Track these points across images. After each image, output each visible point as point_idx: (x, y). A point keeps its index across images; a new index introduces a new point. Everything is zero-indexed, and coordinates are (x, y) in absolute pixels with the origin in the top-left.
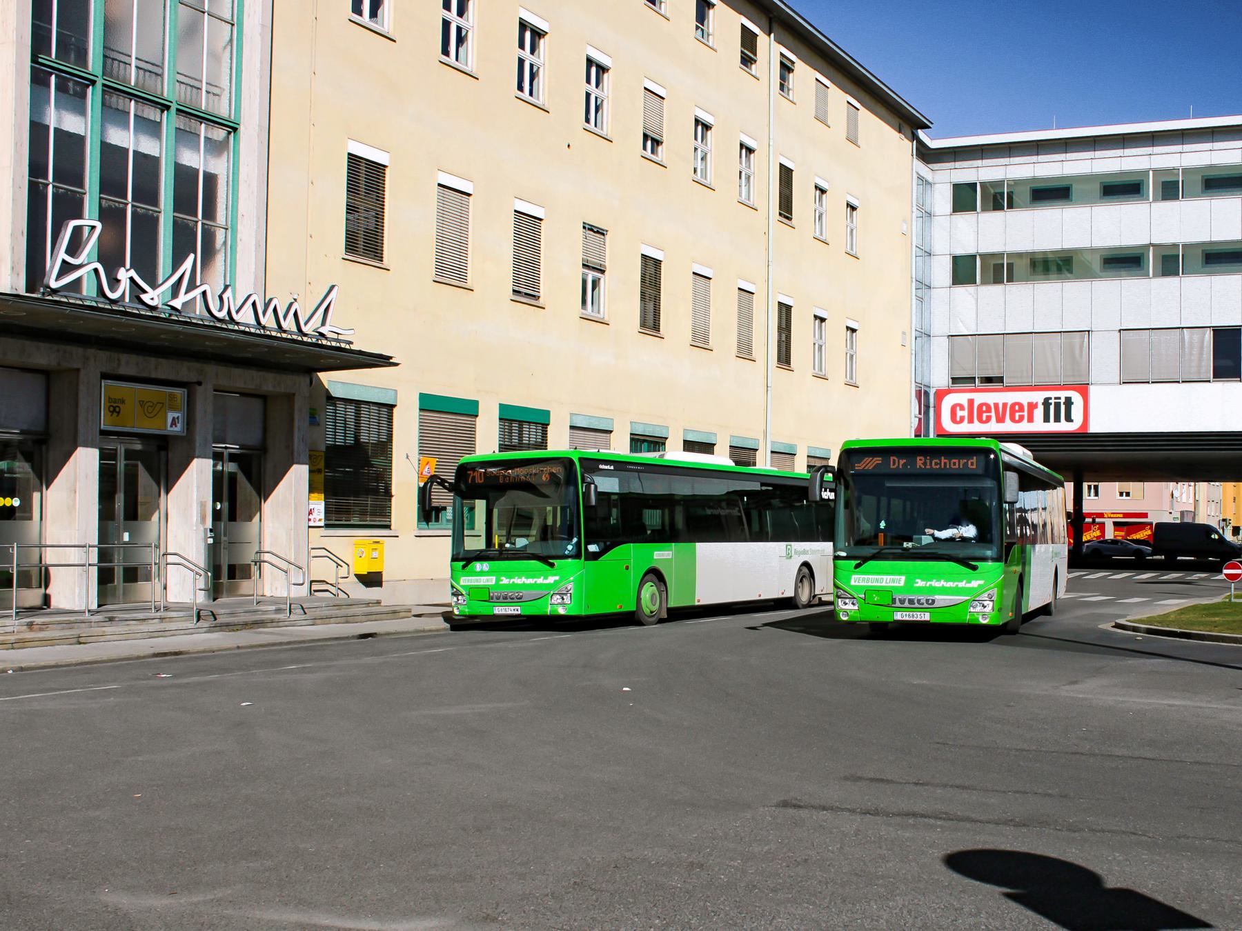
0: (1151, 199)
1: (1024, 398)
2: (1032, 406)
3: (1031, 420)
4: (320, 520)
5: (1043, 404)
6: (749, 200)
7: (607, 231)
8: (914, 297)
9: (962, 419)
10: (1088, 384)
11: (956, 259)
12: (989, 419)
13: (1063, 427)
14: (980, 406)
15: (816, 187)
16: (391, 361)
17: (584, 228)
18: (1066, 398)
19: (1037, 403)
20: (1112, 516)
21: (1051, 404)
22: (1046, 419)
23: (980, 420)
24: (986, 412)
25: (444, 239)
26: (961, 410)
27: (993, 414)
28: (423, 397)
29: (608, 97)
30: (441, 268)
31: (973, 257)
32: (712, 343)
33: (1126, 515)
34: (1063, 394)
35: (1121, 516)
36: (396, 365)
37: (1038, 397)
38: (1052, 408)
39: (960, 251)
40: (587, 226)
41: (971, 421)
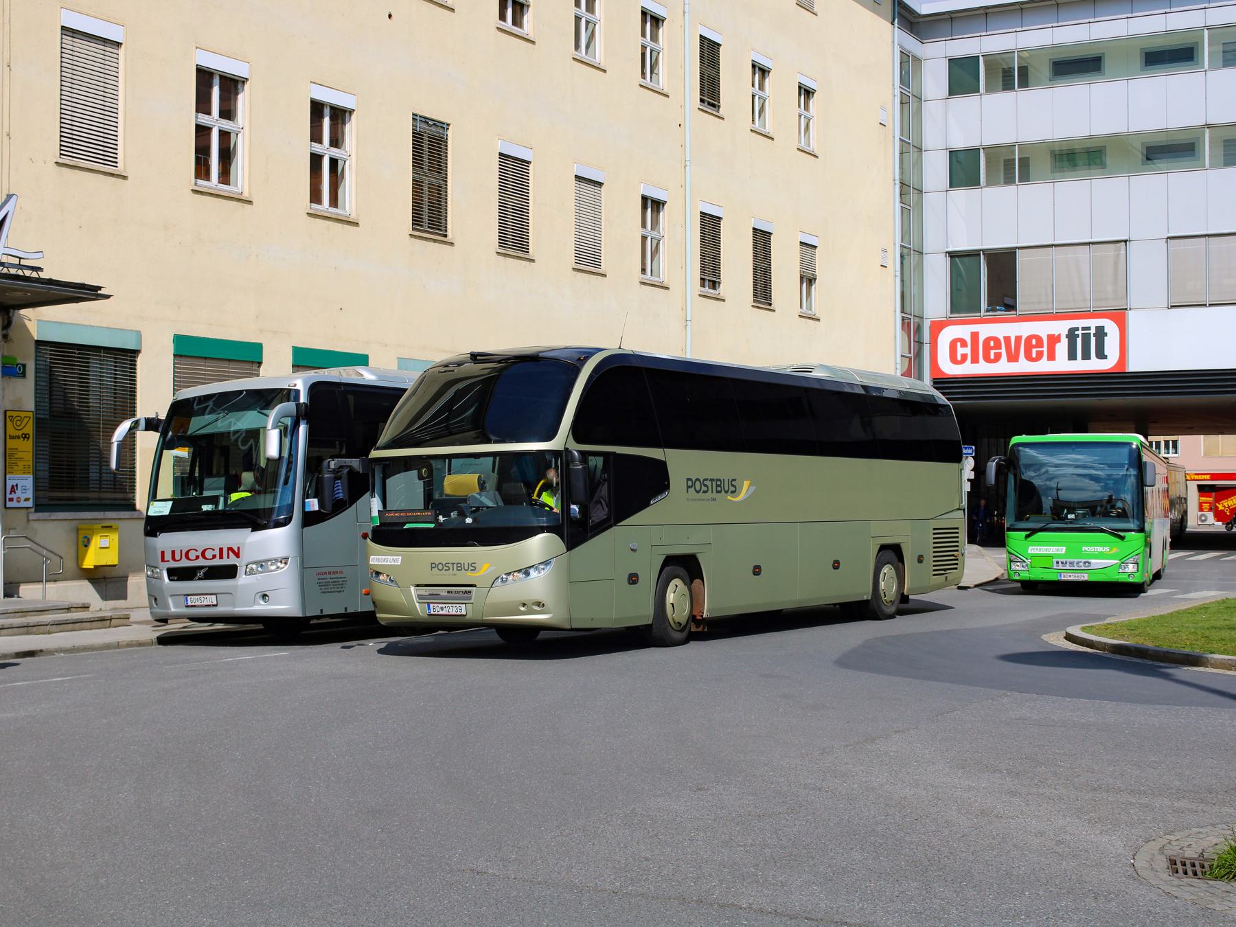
0: (1206, 67)
1: (1044, 329)
2: (1054, 340)
3: (1052, 357)
4: (27, 500)
5: (1067, 336)
7: (448, 125)
9: (964, 357)
10: (1126, 309)
11: (952, 153)
12: (998, 357)
13: (1094, 365)
14: (987, 341)
16: (99, 292)
18: (1097, 328)
19: (1059, 335)
20: (1196, 477)
21: (1078, 335)
22: (1072, 356)
23: (987, 359)
24: (1036, 346)
25: (106, 118)
26: (962, 346)
27: (1003, 351)
28: (179, 340)
30: (579, 257)
31: (974, 152)
33: (1214, 477)
34: (1093, 323)
35: (1208, 477)
36: (107, 297)
37: (1061, 328)
38: (1079, 341)
39: (959, 143)
40: (418, 118)
41: (975, 360)
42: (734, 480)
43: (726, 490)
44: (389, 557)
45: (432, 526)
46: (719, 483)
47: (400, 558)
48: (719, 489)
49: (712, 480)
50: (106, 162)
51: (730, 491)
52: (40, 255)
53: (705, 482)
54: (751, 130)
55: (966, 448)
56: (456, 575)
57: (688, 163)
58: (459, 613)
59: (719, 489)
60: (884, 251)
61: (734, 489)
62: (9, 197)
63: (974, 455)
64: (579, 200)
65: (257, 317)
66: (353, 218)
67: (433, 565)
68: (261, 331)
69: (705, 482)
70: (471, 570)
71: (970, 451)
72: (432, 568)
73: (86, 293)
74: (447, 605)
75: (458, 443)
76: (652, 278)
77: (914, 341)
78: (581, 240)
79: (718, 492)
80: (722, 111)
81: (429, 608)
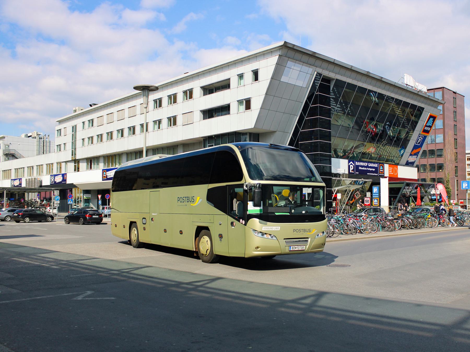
42: (193, 197)
43: (181, 201)
44: (274, 227)
45: (289, 214)
46: (188, 198)
47: (280, 227)
48: (188, 201)
49: (186, 197)
51: (192, 201)
53: (183, 198)
56: (303, 234)
58: (302, 249)
59: (188, 201)
61: (193, 200)
67: (294, 230)
69: (183, 198)
72: (294, 231)
74: (298, 246)
79: (188, 202)
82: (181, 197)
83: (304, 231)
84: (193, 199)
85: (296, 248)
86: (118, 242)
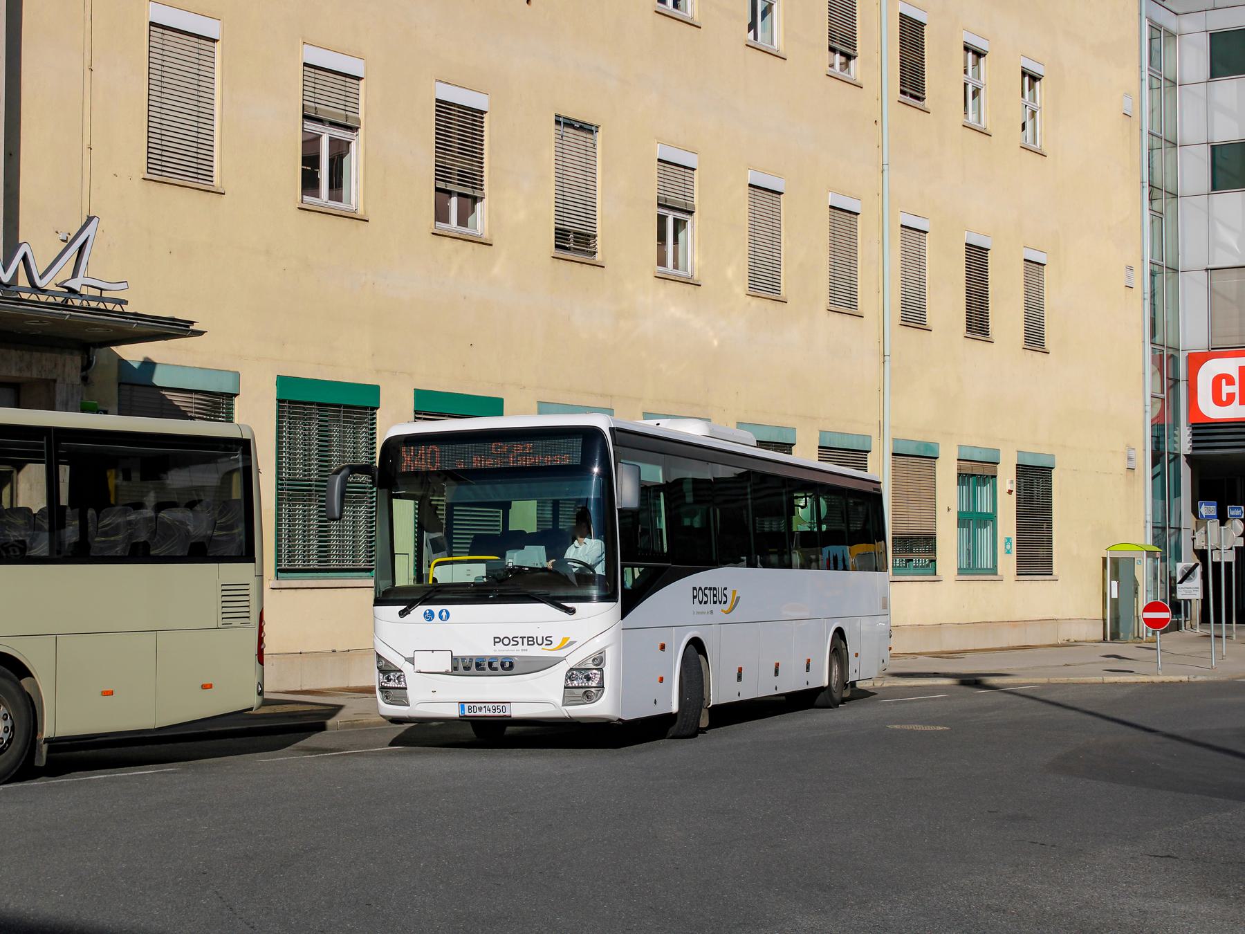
6: (979, 122)
8: (1147, 213)
9: (1231, 397)
11: (1215, 149)
15: (966, 49)
17: (558, 122)
29: (985, 85)
30: (562, 236)
32: (930, 320)
36: (200, 333)
40: (561, 119)
42: (725, 589)
48: (715, 599)
49: (710, 589)
50: (908, 320)
52: (124, 286)
54: (963, 126)
55: (1233, 509)
57: (885, 167)
60: (1130, 268)
62: (90, 219)
63: (1243, 517)
64: (753, 213)
65: (373, 355)
66: (486, 236)
67: (497, 640)
68: (378, 371)
70: (513, 645)
71: (1238, 512)
72: (495, 642)
73: (177, 329)
75: (1042, 553)
76: (676, 272)
77: (1167, 378)
78: (907, 297)
80: (927, 103)
81: (463, 708)
82: (700, 588)
83: (530, 643)
84: (725, 596)
85: (480, 709)
86: (576, 642)
